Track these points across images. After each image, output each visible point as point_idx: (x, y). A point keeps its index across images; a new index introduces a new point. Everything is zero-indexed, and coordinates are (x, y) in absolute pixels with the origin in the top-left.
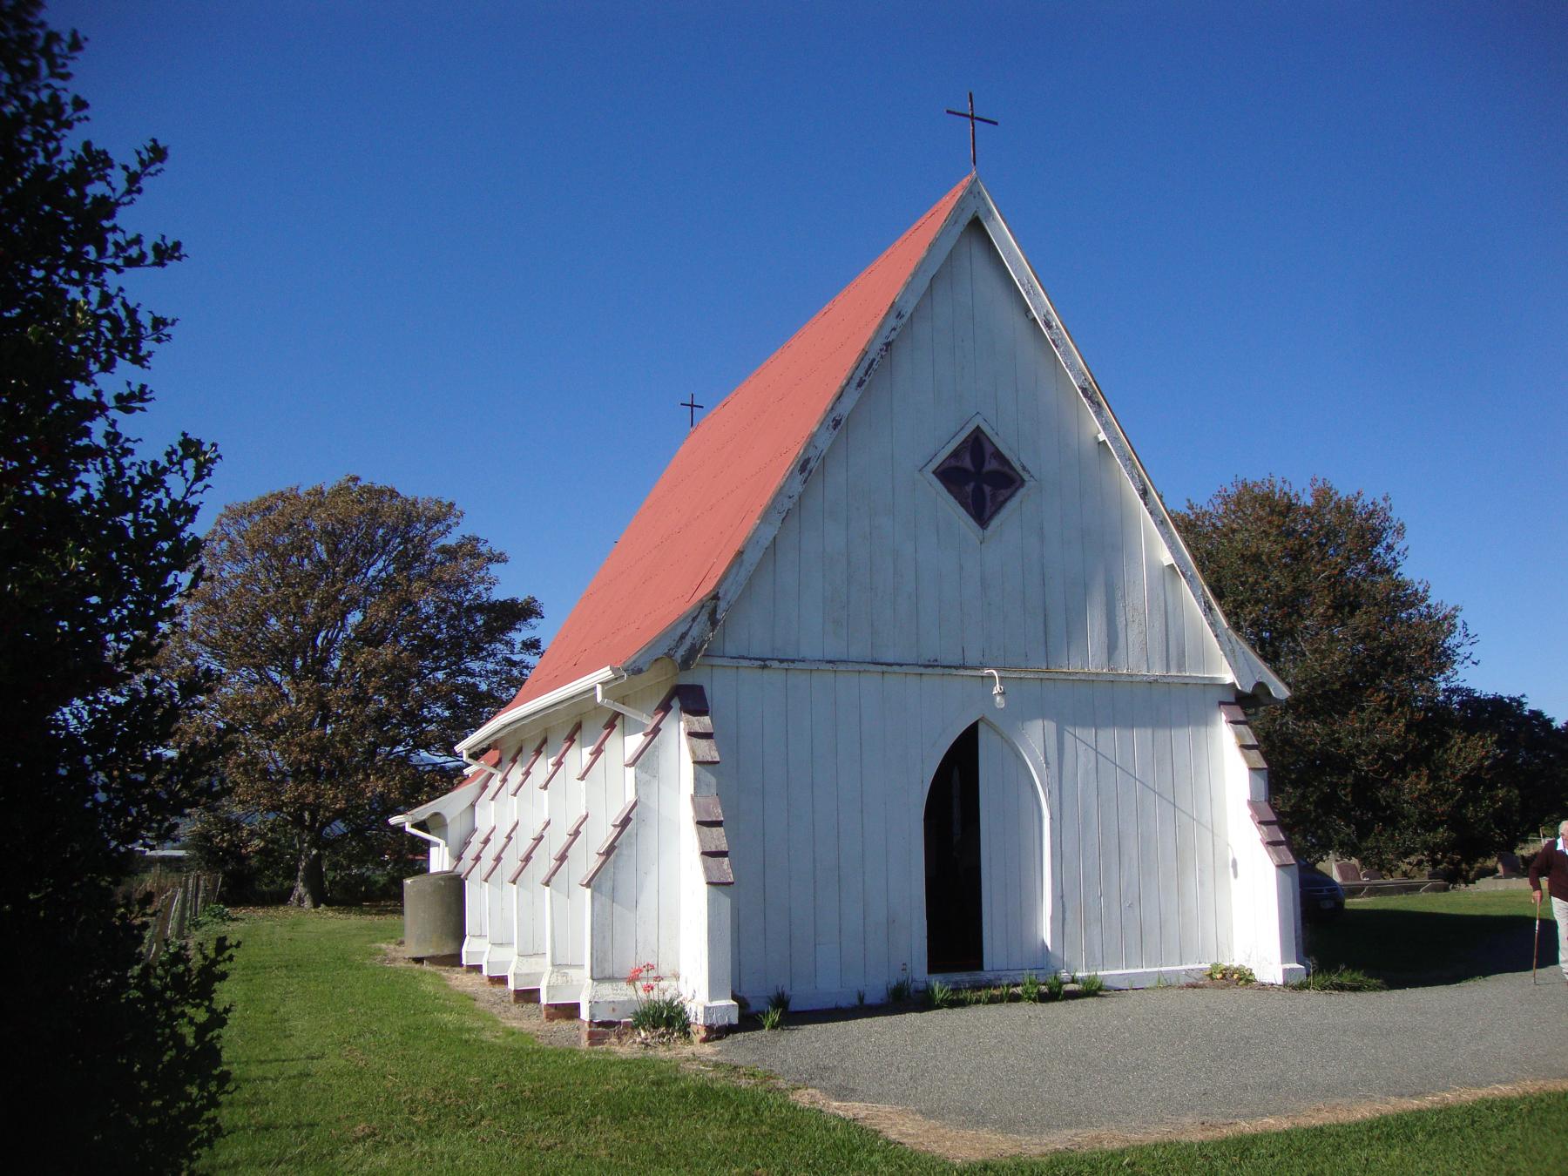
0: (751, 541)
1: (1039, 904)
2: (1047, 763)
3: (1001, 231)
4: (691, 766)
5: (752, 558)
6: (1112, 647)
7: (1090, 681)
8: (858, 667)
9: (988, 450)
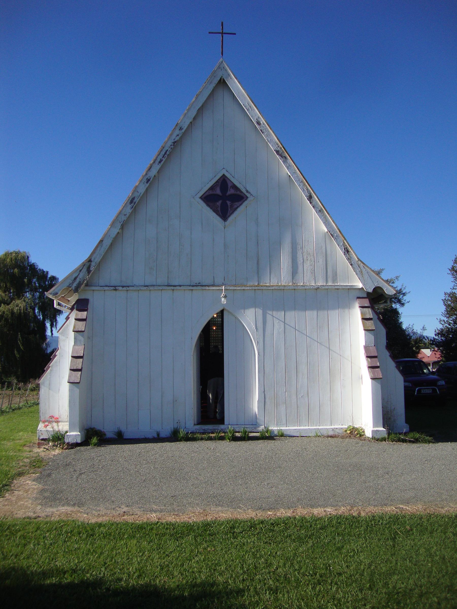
0: (106, 235)
1: (252, 395)
2: (256, 328)
3: (235, 85)
4: (363, 332)
5: (107, 243)
6: (294, 272)
7: (282, 289)
8: (161, 288)
9: (230, 185)
